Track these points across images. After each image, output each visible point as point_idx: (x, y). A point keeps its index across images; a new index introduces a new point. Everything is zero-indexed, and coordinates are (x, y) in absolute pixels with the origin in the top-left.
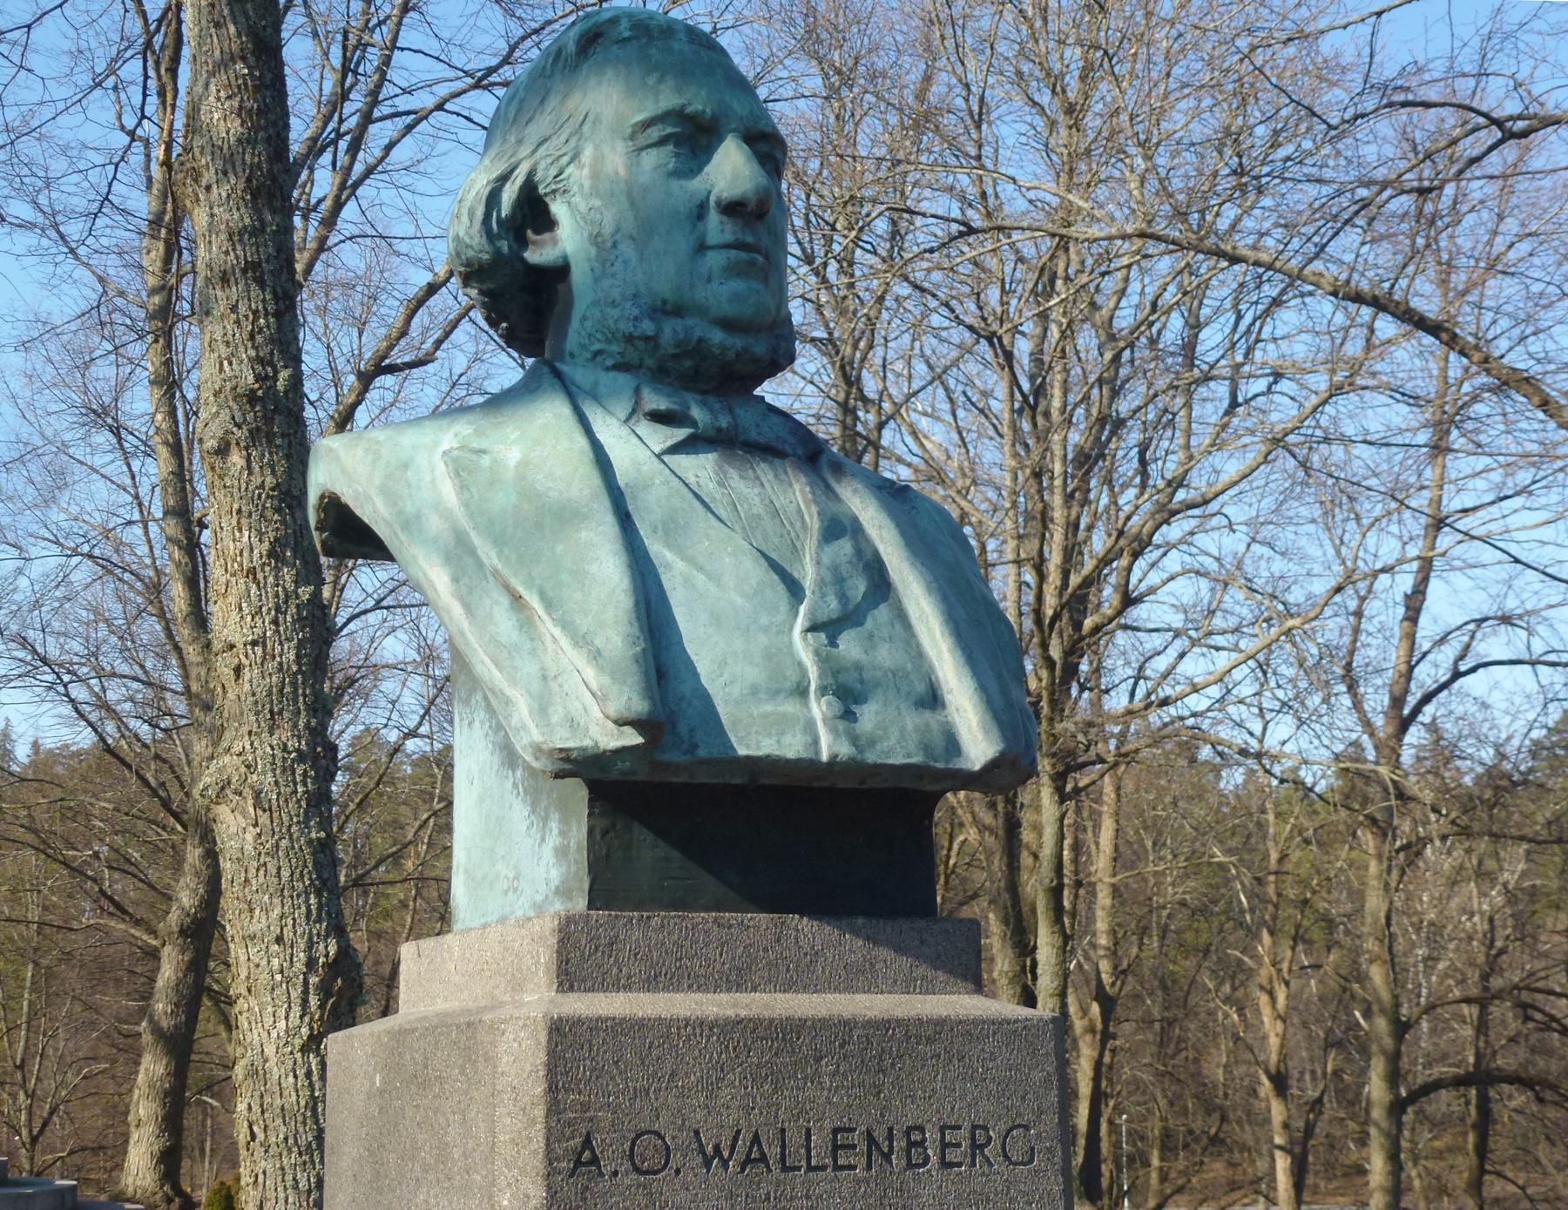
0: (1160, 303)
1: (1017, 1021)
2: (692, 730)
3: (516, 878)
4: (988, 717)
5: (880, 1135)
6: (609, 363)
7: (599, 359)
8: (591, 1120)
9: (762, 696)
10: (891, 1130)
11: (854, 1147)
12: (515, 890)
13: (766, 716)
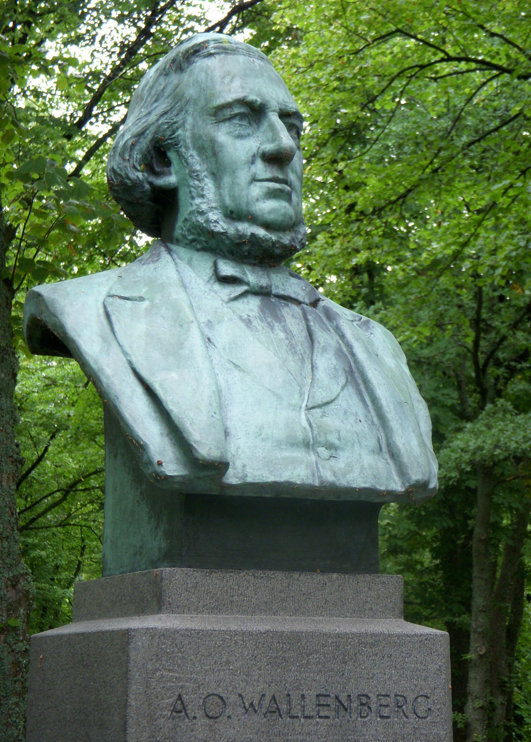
0: (200, 64)
1: (421, 635)
2: (244, 466)
3: (141, 547)
4: (116, 407)
5: (343, 698)
6: (199, 246)
7: (194, 244)
8: (182, 687)
9: (283, 447)
10: (349, 696)
11: (329, 705)
12: (141, 554)
13: (285, 459)
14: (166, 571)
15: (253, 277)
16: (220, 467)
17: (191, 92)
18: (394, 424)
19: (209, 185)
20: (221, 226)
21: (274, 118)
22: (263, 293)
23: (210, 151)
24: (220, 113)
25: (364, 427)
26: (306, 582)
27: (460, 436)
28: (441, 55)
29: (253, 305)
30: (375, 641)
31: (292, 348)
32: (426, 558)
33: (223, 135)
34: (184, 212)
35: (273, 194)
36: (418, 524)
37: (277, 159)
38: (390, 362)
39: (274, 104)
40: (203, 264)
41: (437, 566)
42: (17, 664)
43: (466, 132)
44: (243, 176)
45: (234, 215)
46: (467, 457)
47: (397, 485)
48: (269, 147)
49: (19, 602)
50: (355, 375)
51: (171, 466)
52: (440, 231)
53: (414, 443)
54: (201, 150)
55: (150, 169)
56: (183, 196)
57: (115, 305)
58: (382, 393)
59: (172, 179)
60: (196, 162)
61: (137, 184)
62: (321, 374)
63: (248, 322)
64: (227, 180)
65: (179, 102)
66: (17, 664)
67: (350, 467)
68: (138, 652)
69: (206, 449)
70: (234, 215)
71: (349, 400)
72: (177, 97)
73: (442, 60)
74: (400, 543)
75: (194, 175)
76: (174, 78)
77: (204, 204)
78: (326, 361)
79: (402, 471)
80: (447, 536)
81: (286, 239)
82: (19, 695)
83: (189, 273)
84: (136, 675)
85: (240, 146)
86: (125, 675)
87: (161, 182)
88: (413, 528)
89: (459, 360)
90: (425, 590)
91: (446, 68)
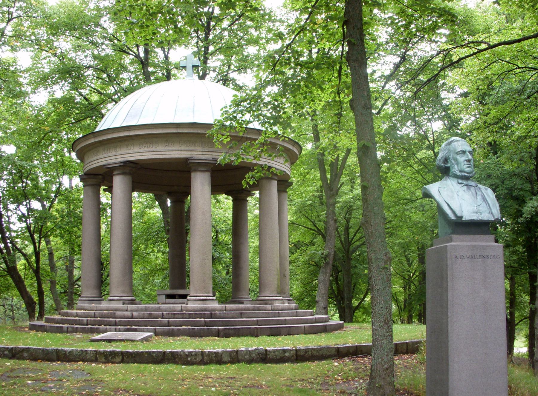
0: (453, 144)
14: (452, 235)
15: (465, 182)
16: (462, 217)
17: (452, 149)
18: (492, 208)
19: (456, 166)
20: (459, 173)
21: (468, 153)
22: (467, 185)
23: (456, 160)
24: (457, 153)
25: (486, 209)
26: (477, 237)
27: (531, 202)
28: (516, 67)
29: (465, 187)
30: (489, 246)
31: (473, 195)
32: (521, 249)
33: (458, 157)
34: (452, 171)
35: (468, 167)
36: (517, 235)
37: (469, 161)
38: (491, 196)
39: (467, 150)
40: (456, 180)
41: (524, 251)
42: (388, 278)
43: (528, 89)
44: (462, 164)
45: (461, 171)
46: (534, 209)
47: (493, 219)
48: (467, 159)
49: (387, 260)
50: (484, 199)
51: (453, 217)
52: (520, 127)
53: (496, 211)
54: (454, 160)
55: (444, 163)
56: (451, 168)
57: (441, 190)
58: (489, 202)
59: (449, 165)
60: (453, 162)
61: (442, 166)
62: (478, 200)
63: (464, 191)
64: (459, 165)
65: (449, 151)
66: (388, 278)
67: (484, 216)
68: (448, 249)
69: (459, 214)
70: (461, 171)
71: (484, 204)
72: (449, 150)
73: (516, 68)
74: (509, 243)
75: (453, 164)
76: (448, 146)
77: (455, 169)
78: (479, 197)
79: (494, 217)
80: (528, 240)
81: (471, 175)
82: (389, 287)
83: (453, 183)
84: (449, 252)
85: (462, 159)
86: (447, 253)
87: (446, 165)
88: (515, 237)
89: (530, 173)
90: (520, 260)
91: (518, 71)
